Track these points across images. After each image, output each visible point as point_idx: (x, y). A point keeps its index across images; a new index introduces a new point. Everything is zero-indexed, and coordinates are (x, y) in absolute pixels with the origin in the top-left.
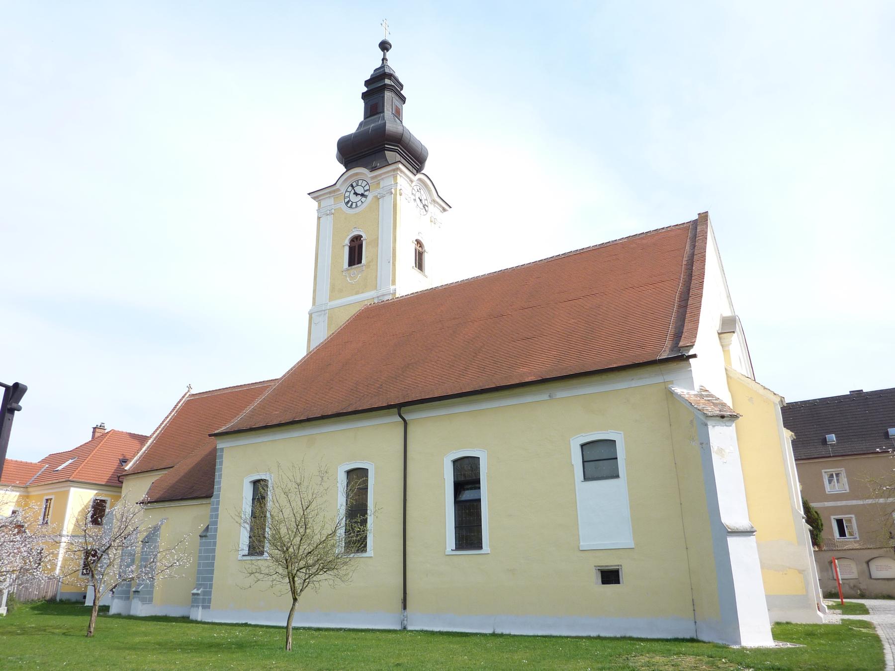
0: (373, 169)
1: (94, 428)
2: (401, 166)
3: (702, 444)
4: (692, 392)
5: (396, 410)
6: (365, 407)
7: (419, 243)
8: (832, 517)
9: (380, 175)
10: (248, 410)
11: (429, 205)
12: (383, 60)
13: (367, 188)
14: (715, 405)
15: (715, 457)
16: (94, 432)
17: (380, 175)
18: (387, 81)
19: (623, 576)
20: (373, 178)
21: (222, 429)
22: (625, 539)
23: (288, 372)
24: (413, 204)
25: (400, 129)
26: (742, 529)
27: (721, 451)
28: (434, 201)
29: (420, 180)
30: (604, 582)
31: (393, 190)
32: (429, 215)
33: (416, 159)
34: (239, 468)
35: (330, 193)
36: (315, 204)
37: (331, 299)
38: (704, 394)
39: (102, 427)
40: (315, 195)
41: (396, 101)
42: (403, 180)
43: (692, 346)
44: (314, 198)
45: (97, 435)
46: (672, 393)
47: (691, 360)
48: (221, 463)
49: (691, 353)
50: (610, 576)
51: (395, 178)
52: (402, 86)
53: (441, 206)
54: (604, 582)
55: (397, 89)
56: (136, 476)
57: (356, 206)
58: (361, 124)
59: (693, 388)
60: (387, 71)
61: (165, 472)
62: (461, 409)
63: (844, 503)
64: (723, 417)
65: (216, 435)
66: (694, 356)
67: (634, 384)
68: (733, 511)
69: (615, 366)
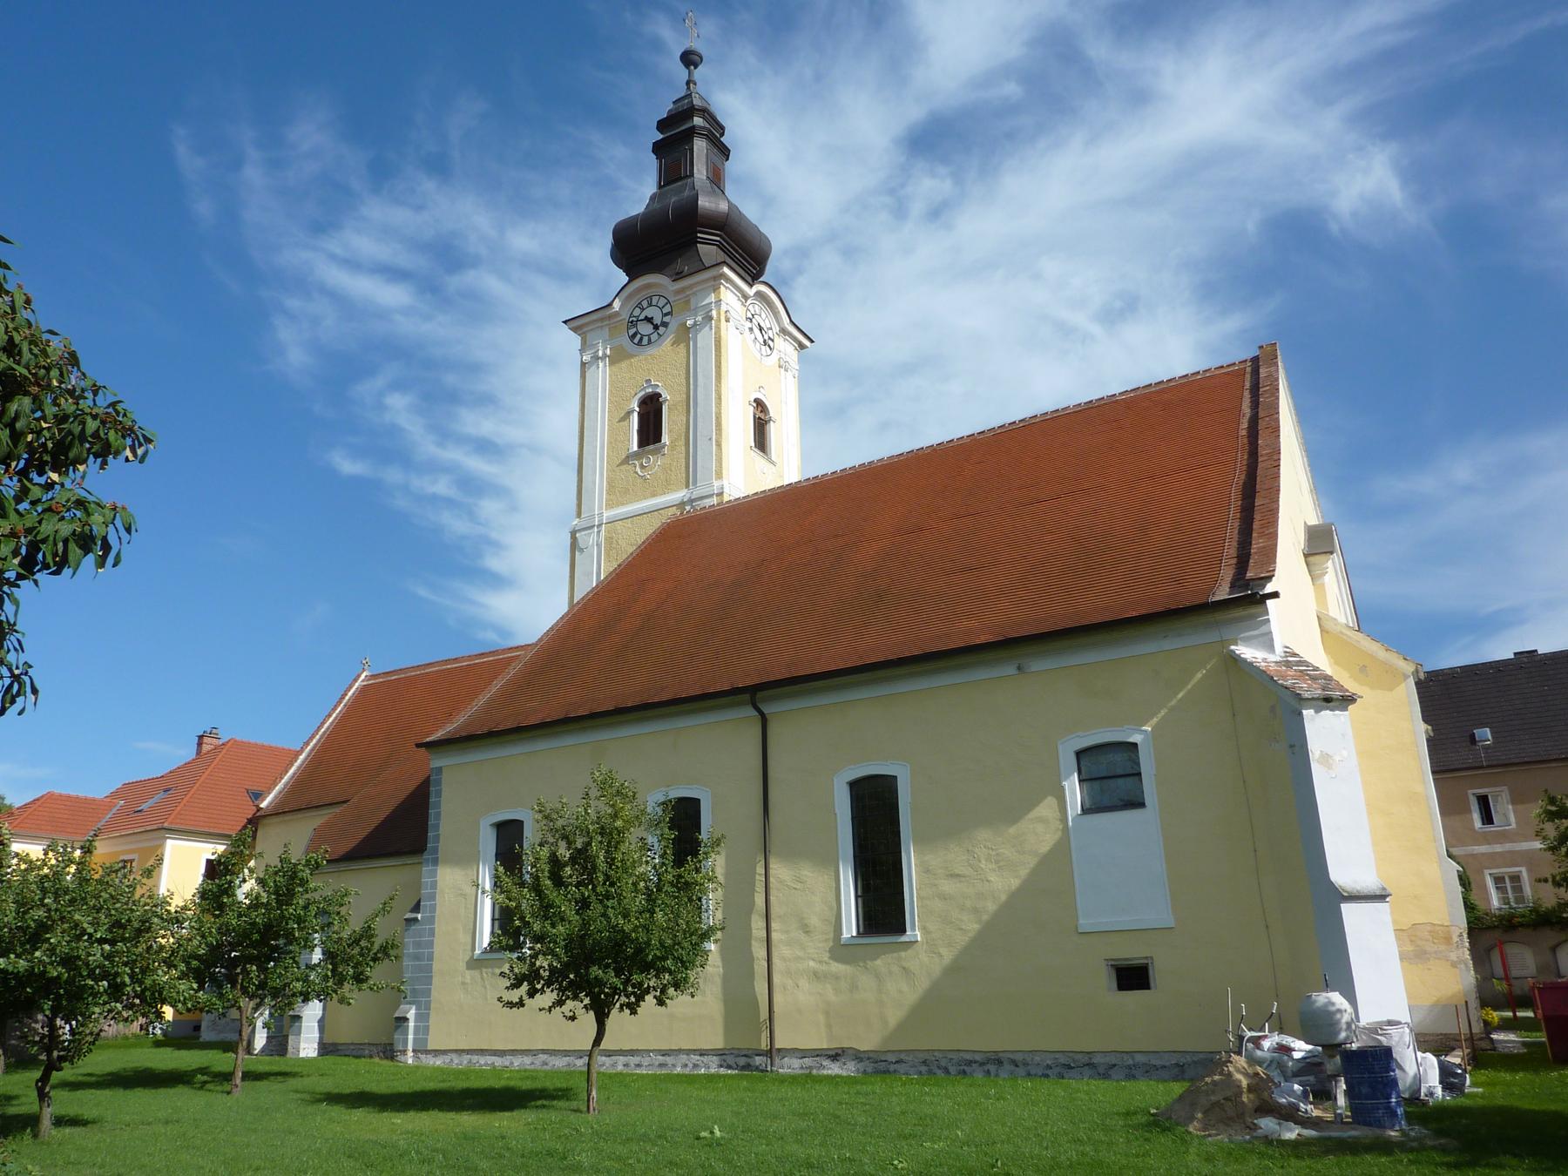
0: (678, 276)
1: (201, 737)
2: (726, 270)
3: (1292, 746)
4: (1272, 658)
5: (747, 697)
6: (692, 693)
7: (759, 404)
8: (1487, 872)
9: (691, 287)
10: (482, 699)
11: (776, 338)
12: (688, 83)
13: (667, 309)
14: (1314, 678)
15: (1315, 767)
16: (200, 744)
17: (691, 287)
18: (698, 121)
19: (1156, 976)
20: (678, 292)
21: (438, 735)
22: (1156, 912)
23: (552, 629)
24: (749, 337)
25: (723, 207)
26: (1365, 891)
27: (1326, 759)
28: (784, 331)
29: (759, 294)
30: (1121, 987)
31: (714, 313)
32: (775, 356)
33: (750, 258)
34: (471, 797)
35: (602, 319)
36: (575, 340)
37: (610, 506)
38: (1291, 660)
39: (212, 733)
40: (576, 324)
41: (717, 158)
42: (731, 299)
43: (1269, 578)
44: (575, 330)
45: (205, 748)
46: (1236, 660)
47: (1270, 603)
48: (439, 794)
49: (1269, 589)
50: (1132, 977)
51: (716, 289)
52: (723, 128)
53: (795, 339)
54: (1121, 987)
55: (715, 134)
56: (281, 818)
57: (650, 342)
58: (652, 198)
59: (1270, 647)
60: (697, 102)
61: (337, 810)
62: (994, 679)
63: (1508, 846)
64: (1328, 700)
65: (429, 745)
66: (1275, 595)
67: (1167, 644)
68: (1349, 860)
69: (1134, 614)
